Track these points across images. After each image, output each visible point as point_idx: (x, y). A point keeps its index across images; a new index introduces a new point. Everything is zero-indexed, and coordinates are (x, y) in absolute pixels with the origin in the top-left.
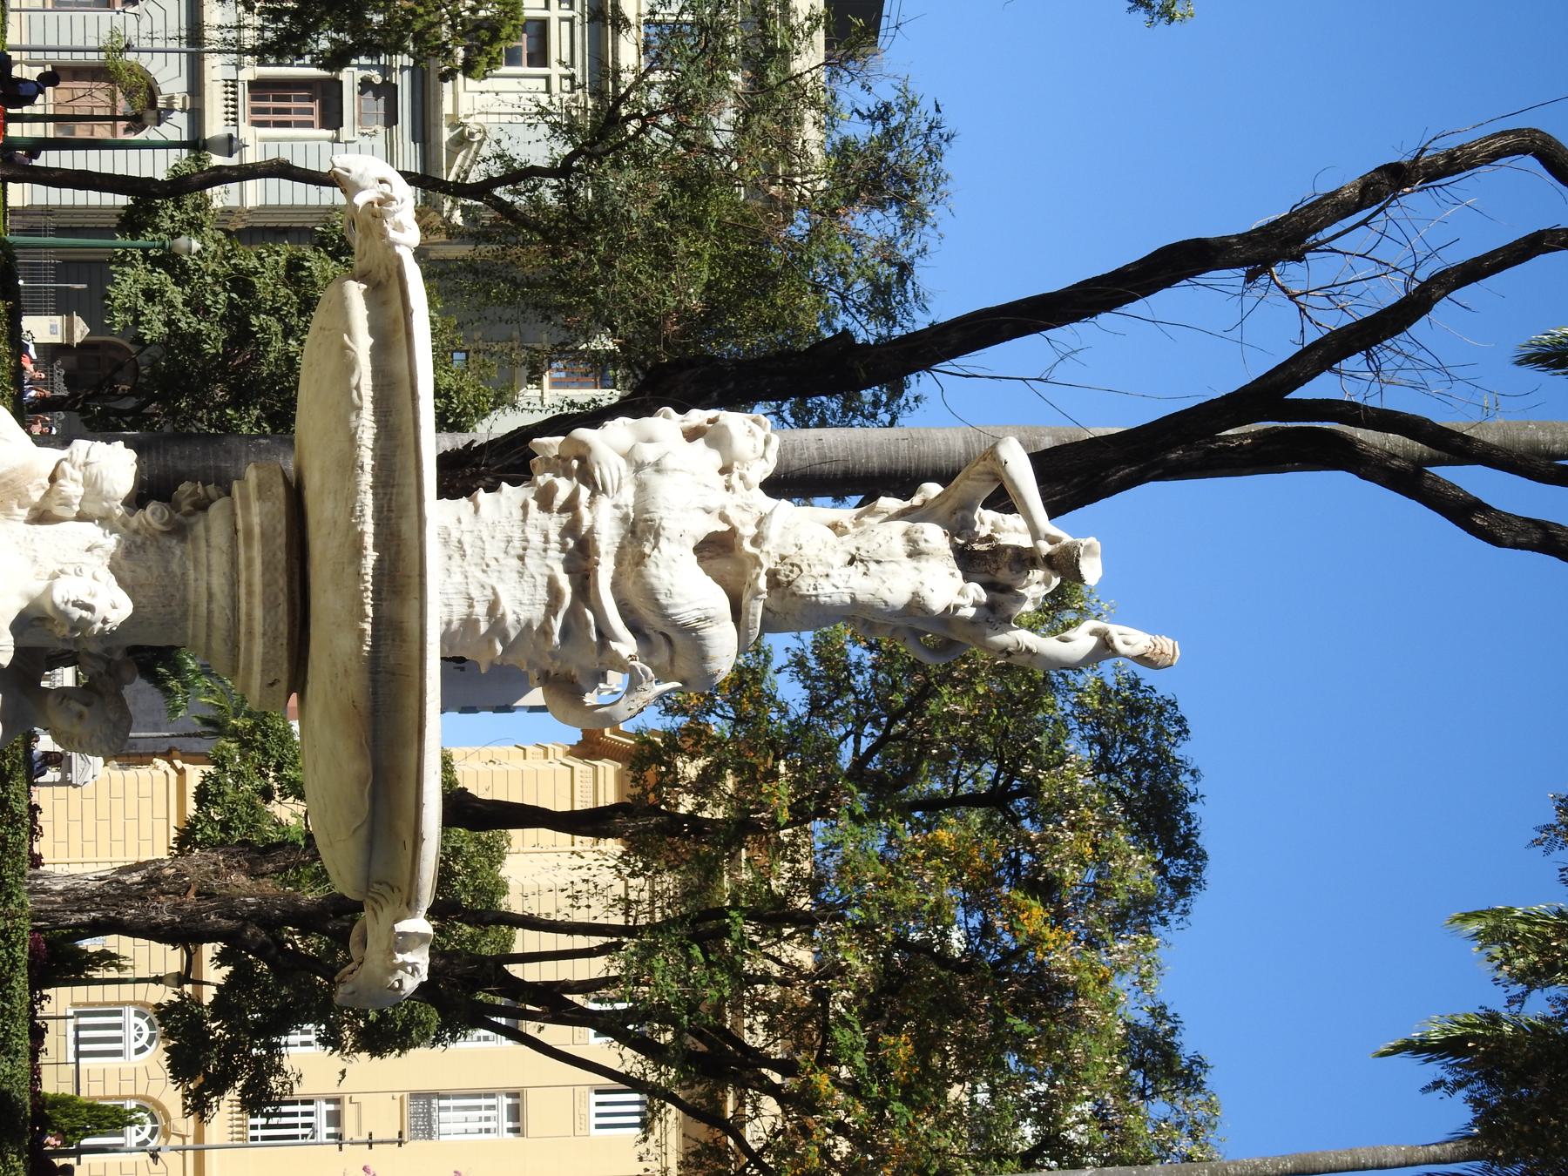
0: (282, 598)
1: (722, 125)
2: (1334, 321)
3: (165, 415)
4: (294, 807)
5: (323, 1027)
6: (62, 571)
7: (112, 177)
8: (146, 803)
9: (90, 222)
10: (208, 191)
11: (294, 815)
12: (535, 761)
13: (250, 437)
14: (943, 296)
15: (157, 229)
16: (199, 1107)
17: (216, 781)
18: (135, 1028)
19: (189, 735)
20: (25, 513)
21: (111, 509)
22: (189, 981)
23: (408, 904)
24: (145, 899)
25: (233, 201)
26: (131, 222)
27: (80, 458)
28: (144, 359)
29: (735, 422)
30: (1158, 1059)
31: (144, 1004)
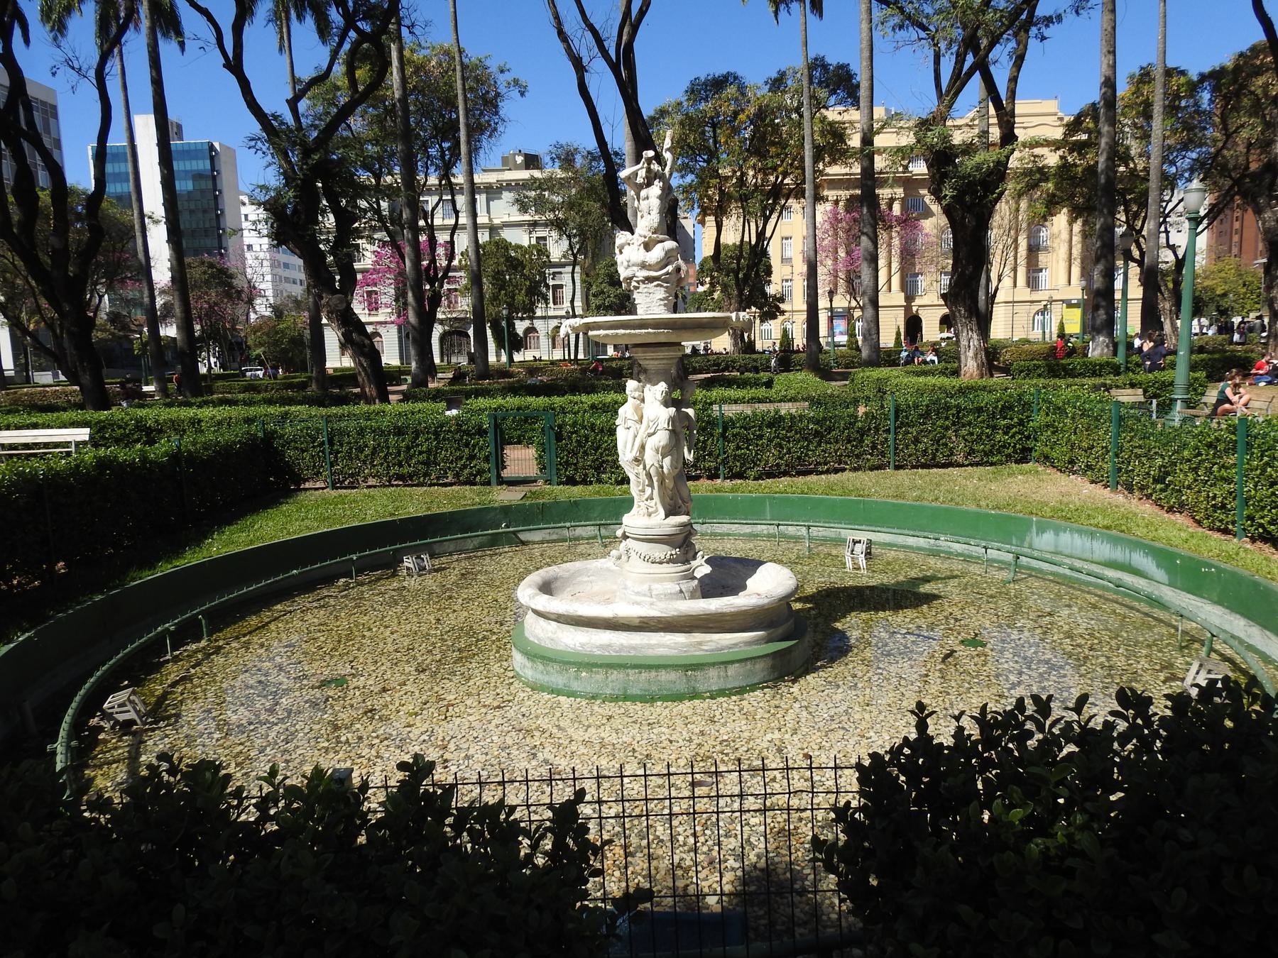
1: (557, 199)
2: (596, 49)
12: (706, 235)
14: (592, 144)
16: (783, 312)
18: (766, 326)
29: (618, 242)
30: (777, 83)
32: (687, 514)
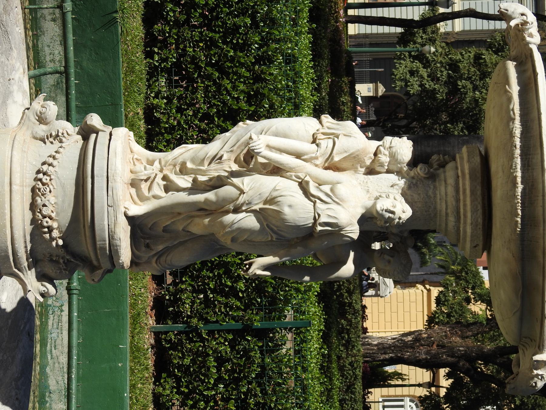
0: (479, 207)
3: (420, 127)
4: (480, 306)
5: (495, 407)
6: (380, 196)
7: (394, 19)
8: (413, 305)
9: (385, 40)
10: (438, 25)
11: (481, 310)
13: (459, 136)
15: (415, 43)
17: (444, 295)
19: (432, 274)
20: (363, 170)
21: (401, 168)
22: (434, 386)
23: (539, 347)
24: (414, 348)
25: (449, 29)
26: (403, 40)
27: (387, 145)
28: (410, 102)
31: (414, 396)
32: (134, 263)
